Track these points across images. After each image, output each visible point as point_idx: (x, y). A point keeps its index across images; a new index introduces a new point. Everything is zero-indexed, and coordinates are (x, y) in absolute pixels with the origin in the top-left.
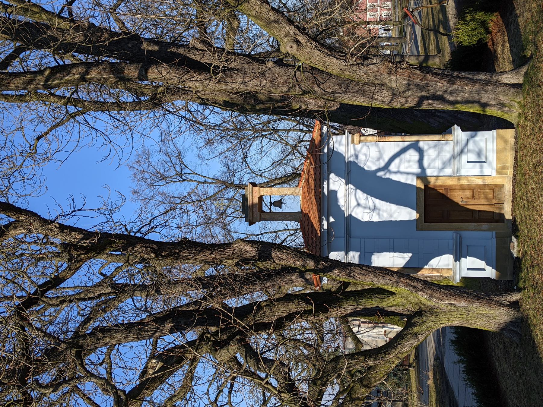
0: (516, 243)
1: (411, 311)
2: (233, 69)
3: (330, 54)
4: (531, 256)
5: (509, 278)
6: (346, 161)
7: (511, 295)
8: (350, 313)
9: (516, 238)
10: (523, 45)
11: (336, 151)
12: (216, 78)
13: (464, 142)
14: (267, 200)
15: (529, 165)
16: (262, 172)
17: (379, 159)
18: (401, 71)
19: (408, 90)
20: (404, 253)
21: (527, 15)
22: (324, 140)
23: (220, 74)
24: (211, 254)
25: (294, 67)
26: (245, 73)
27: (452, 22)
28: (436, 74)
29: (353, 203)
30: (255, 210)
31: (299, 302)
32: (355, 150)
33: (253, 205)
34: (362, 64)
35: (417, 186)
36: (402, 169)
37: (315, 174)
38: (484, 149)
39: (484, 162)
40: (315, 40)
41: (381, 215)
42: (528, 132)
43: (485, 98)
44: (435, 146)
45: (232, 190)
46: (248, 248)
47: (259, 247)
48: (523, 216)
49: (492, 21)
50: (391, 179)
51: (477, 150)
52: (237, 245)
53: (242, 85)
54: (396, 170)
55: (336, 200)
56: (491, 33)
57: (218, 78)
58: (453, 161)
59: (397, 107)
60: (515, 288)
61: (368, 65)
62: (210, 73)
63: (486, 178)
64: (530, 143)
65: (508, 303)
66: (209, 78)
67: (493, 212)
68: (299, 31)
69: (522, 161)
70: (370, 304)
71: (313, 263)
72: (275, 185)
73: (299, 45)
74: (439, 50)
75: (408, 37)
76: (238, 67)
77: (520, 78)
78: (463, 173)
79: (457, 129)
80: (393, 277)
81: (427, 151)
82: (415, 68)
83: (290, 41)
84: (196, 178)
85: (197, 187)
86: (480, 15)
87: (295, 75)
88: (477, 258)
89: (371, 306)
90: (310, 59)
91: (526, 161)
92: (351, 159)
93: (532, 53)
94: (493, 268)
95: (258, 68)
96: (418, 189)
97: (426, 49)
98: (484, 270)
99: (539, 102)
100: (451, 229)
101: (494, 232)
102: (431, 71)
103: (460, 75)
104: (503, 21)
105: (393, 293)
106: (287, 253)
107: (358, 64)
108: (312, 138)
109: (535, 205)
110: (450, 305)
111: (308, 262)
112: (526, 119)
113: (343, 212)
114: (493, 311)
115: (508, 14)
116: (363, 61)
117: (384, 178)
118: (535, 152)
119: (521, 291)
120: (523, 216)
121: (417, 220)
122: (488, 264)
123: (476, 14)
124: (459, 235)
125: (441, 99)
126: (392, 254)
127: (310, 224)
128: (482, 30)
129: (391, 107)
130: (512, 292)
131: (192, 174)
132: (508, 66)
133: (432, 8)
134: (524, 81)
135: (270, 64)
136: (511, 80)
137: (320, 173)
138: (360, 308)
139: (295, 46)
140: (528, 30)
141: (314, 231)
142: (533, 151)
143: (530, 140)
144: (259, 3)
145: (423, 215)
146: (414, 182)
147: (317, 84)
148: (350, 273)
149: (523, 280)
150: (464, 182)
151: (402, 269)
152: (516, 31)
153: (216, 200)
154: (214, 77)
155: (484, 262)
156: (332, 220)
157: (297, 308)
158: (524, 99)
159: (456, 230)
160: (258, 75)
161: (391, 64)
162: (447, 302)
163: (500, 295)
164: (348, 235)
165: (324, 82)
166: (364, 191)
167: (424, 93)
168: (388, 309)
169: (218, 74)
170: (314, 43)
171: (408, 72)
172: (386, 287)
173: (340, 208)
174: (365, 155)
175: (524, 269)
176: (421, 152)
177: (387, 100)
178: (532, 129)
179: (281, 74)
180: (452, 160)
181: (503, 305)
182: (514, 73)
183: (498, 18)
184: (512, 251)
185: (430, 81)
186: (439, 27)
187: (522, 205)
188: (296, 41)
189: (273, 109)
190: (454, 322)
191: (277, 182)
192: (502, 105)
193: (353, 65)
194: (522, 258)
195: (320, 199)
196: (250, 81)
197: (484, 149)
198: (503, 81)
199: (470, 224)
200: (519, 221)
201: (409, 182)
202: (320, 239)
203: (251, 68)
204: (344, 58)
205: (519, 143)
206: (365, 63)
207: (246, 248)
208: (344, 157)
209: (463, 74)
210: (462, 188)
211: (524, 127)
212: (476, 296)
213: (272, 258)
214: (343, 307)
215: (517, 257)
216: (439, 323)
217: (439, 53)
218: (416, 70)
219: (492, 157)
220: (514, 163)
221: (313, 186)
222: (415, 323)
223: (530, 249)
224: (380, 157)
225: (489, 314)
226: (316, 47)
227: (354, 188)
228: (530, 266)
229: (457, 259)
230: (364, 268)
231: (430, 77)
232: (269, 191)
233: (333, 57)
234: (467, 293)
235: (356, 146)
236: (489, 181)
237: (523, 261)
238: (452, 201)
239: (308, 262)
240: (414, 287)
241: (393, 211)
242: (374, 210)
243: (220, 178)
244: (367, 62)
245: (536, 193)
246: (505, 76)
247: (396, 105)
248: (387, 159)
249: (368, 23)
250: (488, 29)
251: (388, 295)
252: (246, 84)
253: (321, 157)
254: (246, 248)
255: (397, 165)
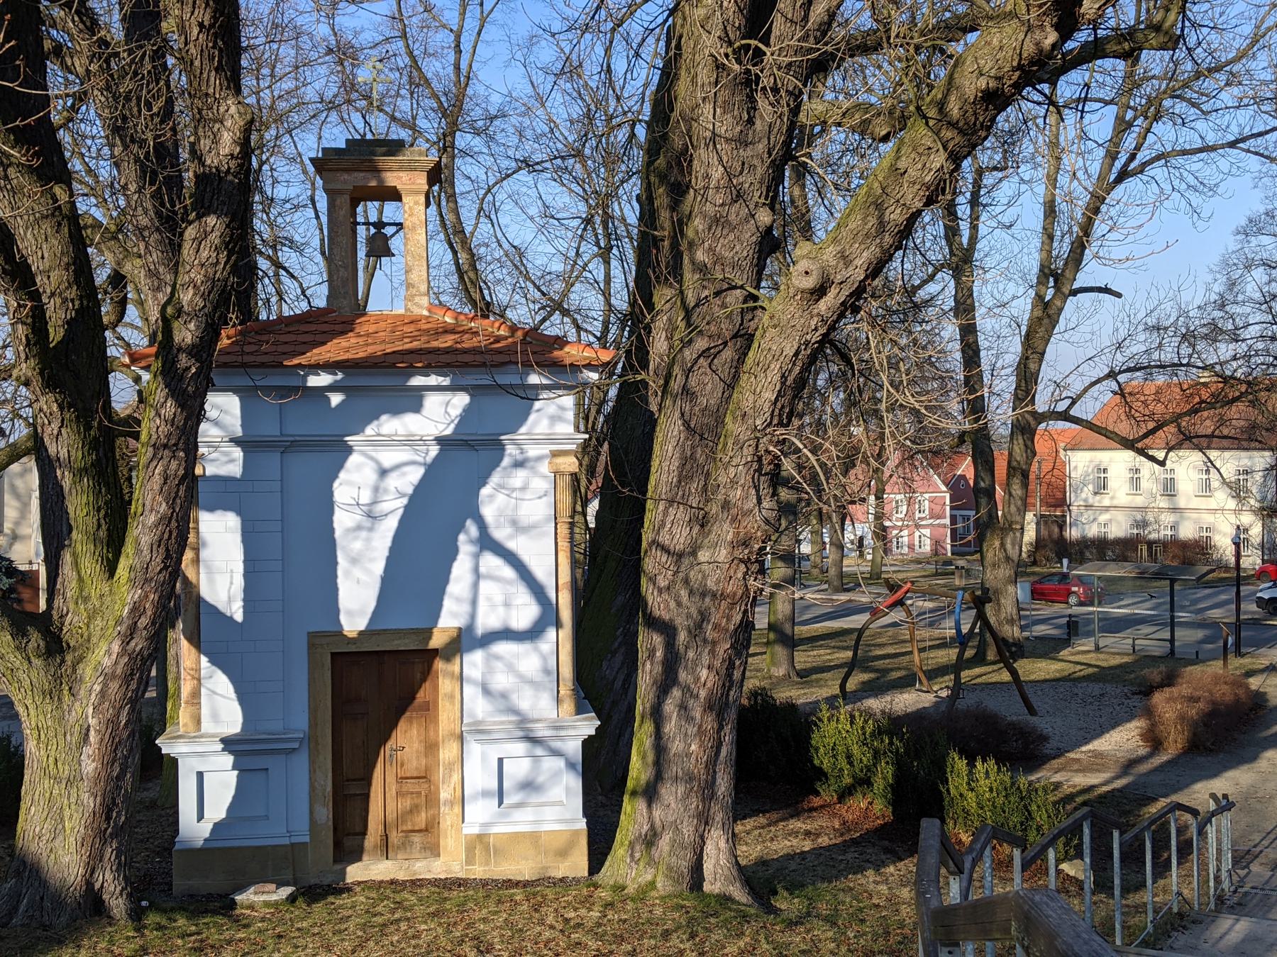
0: (274, 897)
1: (63, 624)
2: (753, 107)
3: (788, 383)
4: (229, 943)
5: (179, 884)
6: (503, 437)
7: (121, 894)
8: (46, 450)
9: (287, 899)
10: (802, 886)
11: (531, 407)
12: (727, 55)
13: (557, 744)
14: (391, 211)
15: (485, 920)
16: (493, 217)
17: (514, 523)
18: (740, 575)
19: (691, 593)
20: (245, 600)
21: (879, 892)
22: (563, 373)
23: (736, 67)
24: (201, 25)
25: (754, 285)
26: (742, 141)
27: (874, 704)
28: (731, 666)
29: (389, 457)
30: (357, 178)
31: (72, 301)
32: (539, 459)
33: (376, 171)
34: (759, 470)
35: (435, 630)
36: (484, 586)
37: (465, 351)
38: (543, 799)
39: (501, 803)
40: (826, 339)
41: (356, 534)
42: (572, 915)
43: (671, 794)
44: (547, 672)
45: (436, 125)
46: (227, 142)
47: (230, 178)
48: (350, 912)
49: (871, 803)
50: (454, 559)
51: (541, 779)
52: (233, 109)
53: (708, 134)
54: (482, 570)
55: (396, 411)
56: (840, 803)
57: (727, 62)
58: (510, 722)
59: (645, 567)
60: (144, 903)
61: (755, 487)
62: (742, 39)
63: (457, 809)
64: (542, 922)
65: (97, 886)
66: (728, 35)
67: (364, 833)
68: (851, 295)
69: (499, 902)
70: (79, 505)
71: (189, 340)
72: (455, 253)
73: (812, 294)
74: (805, 675)
75: (843, 597)
76: (758, 122)
77: (718, 884)
78: (474, 749)
79: (588, 726)
80: (160, 572)
81: (536, 649)
82: (746, 611)
83: (823, 269)
84: (471, 24)
85: (444, 26)
86: (885, 773)
87: (735, 287)
88: (234, 797)
89: (71, 510)
90: (775, 326)
91: (496, 913)
92: (510, 450)
93: (781, 910)
94: (205, 840)
95: (752, 182)
96: (427, 633)
97: (813, 640)
98: (201, 817)
99: (651, 937)
100: (313, 723)
101: (307, 839)
102: (739, 654)
103: (727, 729)
104: (868, 831)
105: (111, 568)
106: (218, 262)
107: (760, 459)
108: (568, 343)
109: (371, 944)
110: (83, 731)
111: (192, 326)
112: (609, 905)
113: (359, 430)
114: (73, 849)
115: (886, 843)
116: (766, 474)
117: (456, 540)
118: (517, 935)
119: (133, 921)
120: (350, 912)
121: (339, 633)
122: (217, 826)
123: (887, 763)
124: (296, 745)
125: (667, 681)
126: (240, 568)
127: (319, 338)
128: (847, 780)
129: (646, 552)
130: (130, 895)
131: (482, 12)
132: (750, 852)
133: (911, 653)
134: (709, 895)
135: (764, 217)
136: (713, 861)
137: (466, 365)
138: (67, 481)
139: (810, 283)
140: (841, 896)
141: (299, 348)
142: (521, 930)
143: (550, 920)
144: (928, 179)
145: (353, 649)
146: (450, 619)
147: (709, 349)
148: (165, 446)
149: (164, 922)
150: (448, 752)
151: (195, 594)
152: (842, 867)
153: (411, 83)
154: (729, 50)
155: (223, 815)
156: (336, 399)
157: (53, 294)
158: (662, 898)
159: (312, 740)
160: (735, 182)
161: (757, 546)
162: (93, 722)
163: (119, 864)
164: (289, 446)
165: (714, 368)
166: (419, 488)
167: (682, 636)
168: (67, 557)
169: (739, 62)
170: (816, 337)
171: (735, 594)
172: (129, 548)
173: (369, 422)
174: (524, 488)
175: (196, 925)
176: (532, 634)
177: (664, 538)
178: (579, 925)
179: (739, 246)
180: (514, 718)
181: (91, 875)
182: (729, 868)
183: (878, 818)
184: (252, 889)
185: (712, 653)
186: (866, 669)
187: (379, 909)
188: (822, 286)
189: (653, 235)
190: (35, 742)
191: (463, 257)
192: (650, 840)
193: (757, 446)
194: (231, 916)
195: (393, 366)
196: (720, 160)
197: (543, 799)
198: (708, 842)
199: (330, 775)
200: (337, 902)
201: (448, 604)
202: (273, 367)
203: (755, 162)
204: (775, 421)
205: (548, 891)
206: (762, 478)
207: (226, 137)
208: (514, 431)
209: (728, 736)
210: (431, 748)
211: (587, 902)
212: (113, 799)
213: (199, 217)
214: (63, 430)
215: (236, 904)
216: (29, 702)
217: (798, 674)
218: (741, 615)
219: (522, 821)
220: (496, 880)
221: (435, 344)
222: (24, 634)
223: (252, 937)
224: (519, 527)
225: (61, 838)
226: (807, 343)
227: (429, 459)
228: (202, 941)
229: (229, 744)
230: (183, 488)
231: (722, 652)
232: (414, 219)
233: (779, 391)
234: (120, 777)
235: (546, 462)
236: (448, 817)
237: (220, 920)
238: (394, 725)
239: (192, 326)
240: (133, 629)
241: (369, 565)
242: (370, 515)
243: (470, 91)
244: (764, 483)
245: (403, 945)
246: (722, 844)
247: (653, 562)
248: (511, 545)
249: (879, 497)
250: (851, 794)
251: (107, 558)
252: (711, 147)
253: (514, 367)
254: (226, 137)
255: (498, 573)
